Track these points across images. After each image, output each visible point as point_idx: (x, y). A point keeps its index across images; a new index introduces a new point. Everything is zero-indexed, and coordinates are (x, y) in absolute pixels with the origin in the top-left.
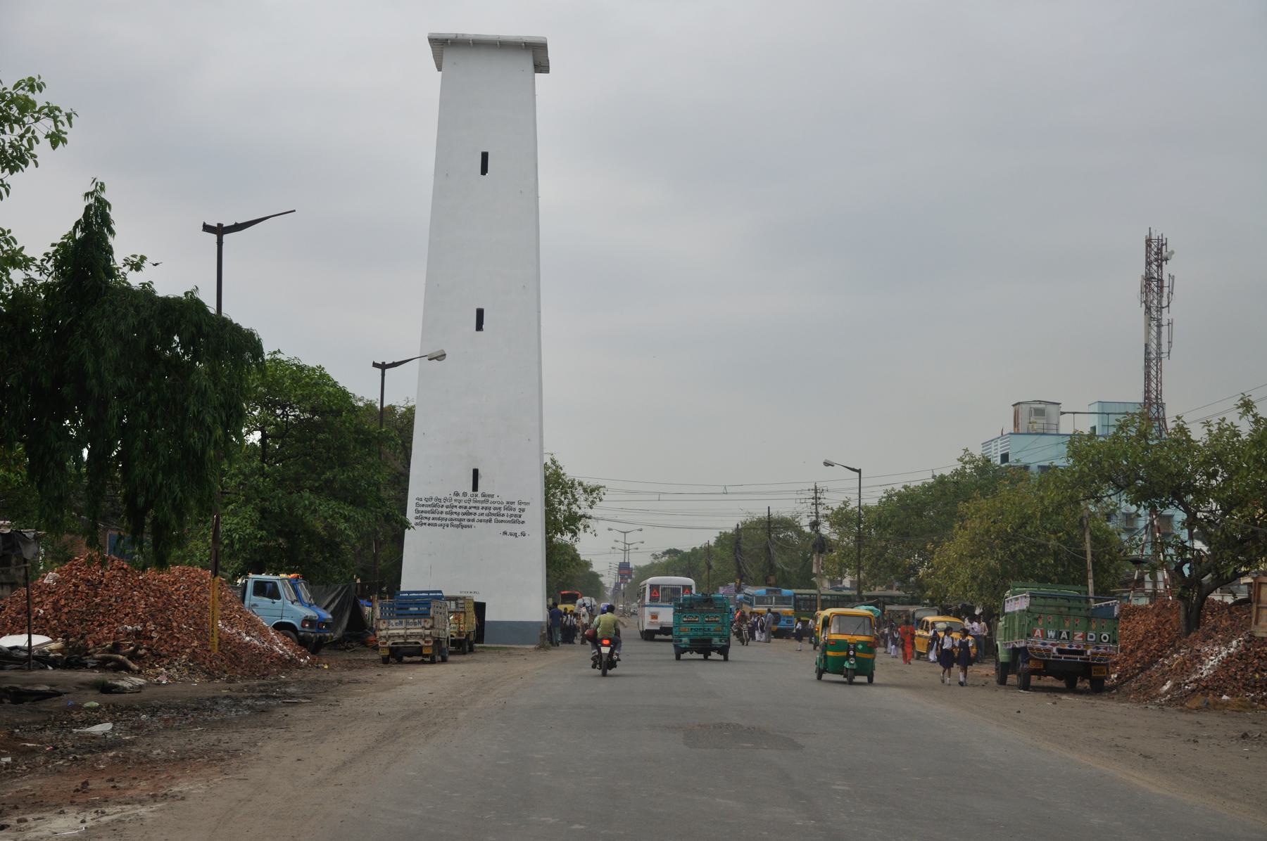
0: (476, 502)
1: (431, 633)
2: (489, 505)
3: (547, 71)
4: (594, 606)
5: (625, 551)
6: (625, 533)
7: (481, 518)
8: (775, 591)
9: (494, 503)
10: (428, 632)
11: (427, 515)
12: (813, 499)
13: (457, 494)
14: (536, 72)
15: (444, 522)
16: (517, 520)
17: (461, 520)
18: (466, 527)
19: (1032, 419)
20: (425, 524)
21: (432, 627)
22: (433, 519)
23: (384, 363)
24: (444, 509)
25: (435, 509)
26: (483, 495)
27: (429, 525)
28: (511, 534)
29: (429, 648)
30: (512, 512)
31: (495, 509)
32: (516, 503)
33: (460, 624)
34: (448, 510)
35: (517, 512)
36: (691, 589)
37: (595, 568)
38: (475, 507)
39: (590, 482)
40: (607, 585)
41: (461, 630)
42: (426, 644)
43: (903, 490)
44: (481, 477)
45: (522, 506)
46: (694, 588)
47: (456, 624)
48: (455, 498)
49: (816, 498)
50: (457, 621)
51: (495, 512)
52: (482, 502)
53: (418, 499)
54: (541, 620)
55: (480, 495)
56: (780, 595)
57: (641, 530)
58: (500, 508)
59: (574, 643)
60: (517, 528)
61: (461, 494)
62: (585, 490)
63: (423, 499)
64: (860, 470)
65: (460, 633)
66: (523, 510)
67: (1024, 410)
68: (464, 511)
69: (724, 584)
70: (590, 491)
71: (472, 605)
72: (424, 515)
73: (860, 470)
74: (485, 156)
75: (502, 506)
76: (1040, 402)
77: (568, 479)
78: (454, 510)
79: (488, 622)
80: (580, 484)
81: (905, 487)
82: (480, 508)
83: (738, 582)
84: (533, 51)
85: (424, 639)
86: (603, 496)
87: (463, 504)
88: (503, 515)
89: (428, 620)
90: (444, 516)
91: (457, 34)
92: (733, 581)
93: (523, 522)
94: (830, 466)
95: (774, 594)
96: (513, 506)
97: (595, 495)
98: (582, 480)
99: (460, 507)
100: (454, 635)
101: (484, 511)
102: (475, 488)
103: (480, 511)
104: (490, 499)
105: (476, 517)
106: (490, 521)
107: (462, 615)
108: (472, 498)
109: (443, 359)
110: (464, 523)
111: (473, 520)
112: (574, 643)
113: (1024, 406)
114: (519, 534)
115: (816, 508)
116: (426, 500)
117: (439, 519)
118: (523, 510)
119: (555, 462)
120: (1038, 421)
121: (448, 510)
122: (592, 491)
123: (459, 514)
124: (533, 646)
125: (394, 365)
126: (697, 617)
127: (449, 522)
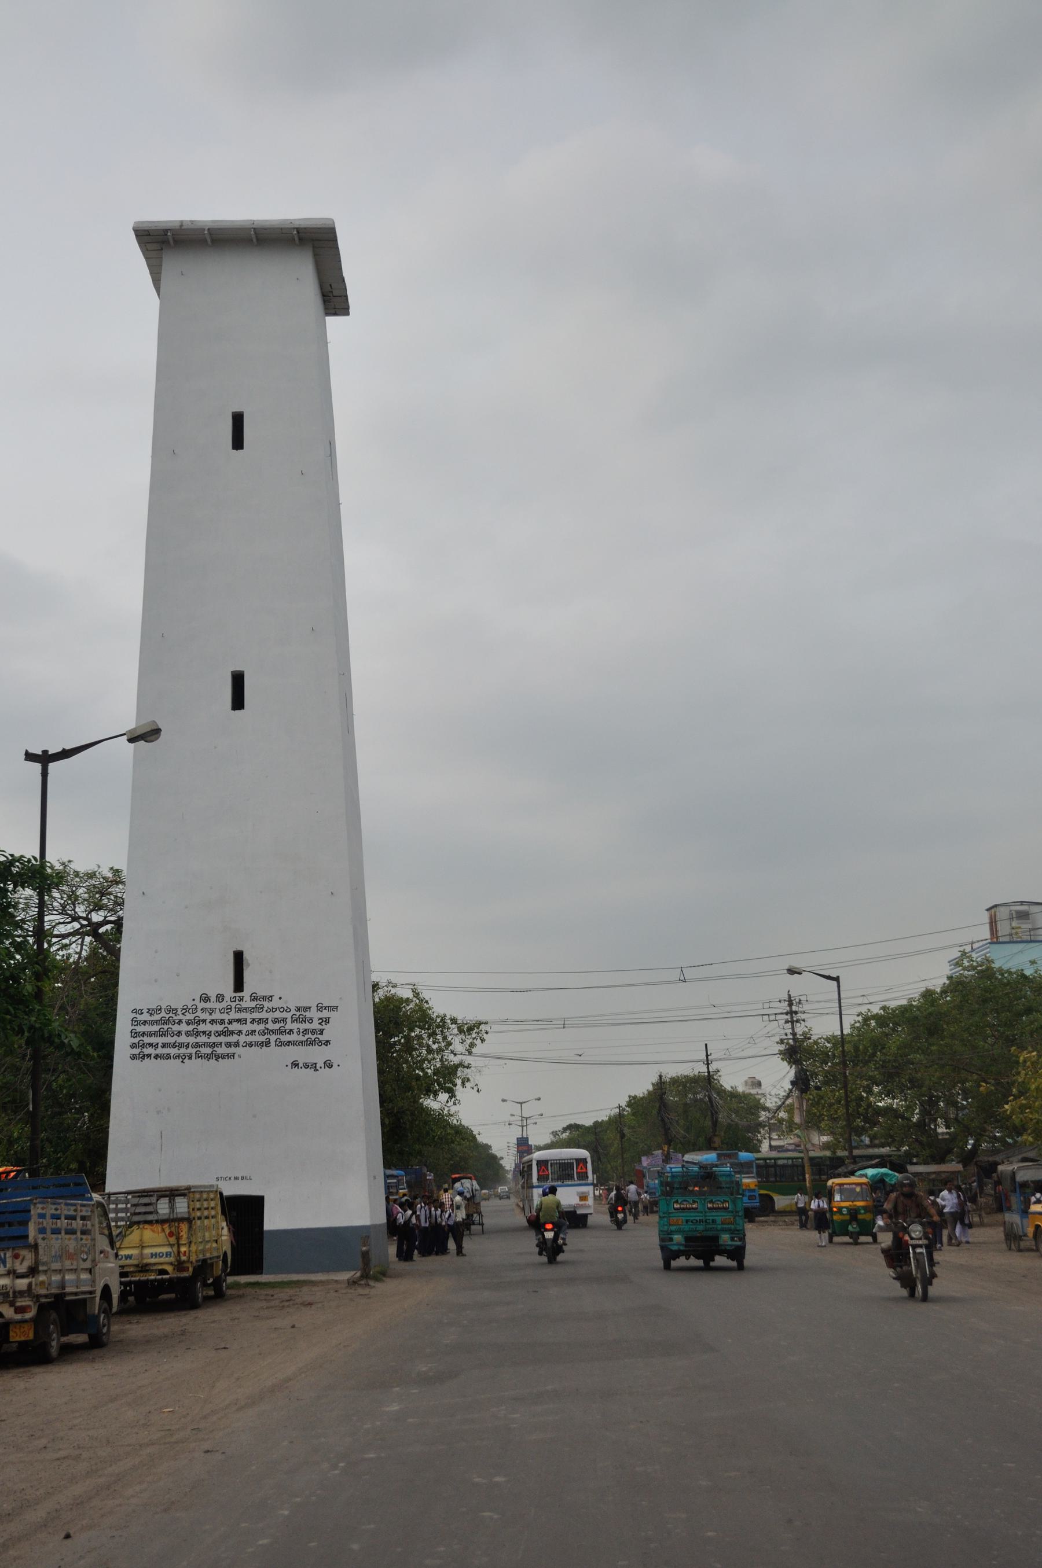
0: (240, 1010)
1: (30, 1285)
2: (263, 1015)
3: (347, 314)
4: (476, 1190)
5: (523, 1126)
6: (521, 1103)
7: (250, 1039)
8: (729, 1156)
9: (273, 1010)
10: (22, 1283)
11: (153, 1040)
12: (787, 1014)
13: (205, 998)
14: (328, 314)
15: (183, 1051)
16: (315, 1039)
17: (213, 1045)
18: (223, 1056)
19: (1014, 924)
20: (149, 1056)
21: (33, 1271)
22: (164, 1046)
23: (45, 752)
24: (184, 1027)
25: (166, 1027)
26: (254, 998)
27: (157, 1057)
28: (306, 1066)
29: (26, 1326)
30: (307, 1026)
31: (276, 1021)
32: (314, 1009)
33: (179, 1246)
34: (191, 1028)
35: (315, 1025)
36: (587, 1162)
37: (495, 1150)
38: (239, 1021)
39: (466, 1014)
40: (508, 1168)
41: (183, 1258)
42: (18, 1317)
43: (882, 1012)
44: (249, 965)
45: (325, 1014)
46: (589, 1161)
47: (171, 1245)
48: (203, 1005)
49: (791, 1013)
50: (173, 1240)
51: (277, 1026)
52: (252, 1010)
53: (135, 1011)
54: (367, 1222)
55: (247, 998)
56: (736, 1161)
57: (536, 1123)
58: (284, 1020)
59: (648, 1090)
60: (316, 1054)
61: (213, 999)
62: (461, 1031)
63: (145, 1011)
64: (838, 977)
65: (180, 1266)
66: (327, 1021)
67: (1003, 913)
68: (220, 1028)
69: (648, 1153)
70: (469, 1029)
71: (216, 1203)
72: (147, 1040)
73: (838, 977)
74: (238, 420)
75: (288, 1015)
76: (1022, 903)
77: (435, 1014)
78: (202, 1027)
79: (271, 1232)
80: (454, 1021)
81: (884, 1008)
82: (249, 1021)
83: (666, 1149)
84: (314, 247)
85: (12, 1304)
86: (485, 1035)
87: (217, 1016)
88: (291, 1031)
89: (23, 1253)
90: (183, 1039)
91: (182, 222)
92: (660, 1147)
93: (327, 1043)
94: (796, 975)
95: (728, 1160)
96: (308, 1014)
97: (474, 1035)
98: (455, 1015)
99: (212, 1022)
100: (169, 1268)
101: (256, 1027)
102: (239, 986)
103: (249, 1027)
104: (266, 1004)
105: (242, 1039)
106: (267, 1044)
107: (184, 1227)
108: (233, 1005)
109: (157, 739)
110: (220, 1050)
111: (237, 1045)
112: (648, 1090)
113: (1002, 909)
114: (320, 1064)
115: (793, 1028)
116: (151, 1012)
117: (174, 1046)
118: (327, 1021)
119: (418, 994)
120: (1023, 926)
121: (191, 1028)
122: (470, 1029)
123: (210, 1035)
124: (345, 1276)
125: (65, 754)
126: (694, 1202)
127: (193, 1051)
